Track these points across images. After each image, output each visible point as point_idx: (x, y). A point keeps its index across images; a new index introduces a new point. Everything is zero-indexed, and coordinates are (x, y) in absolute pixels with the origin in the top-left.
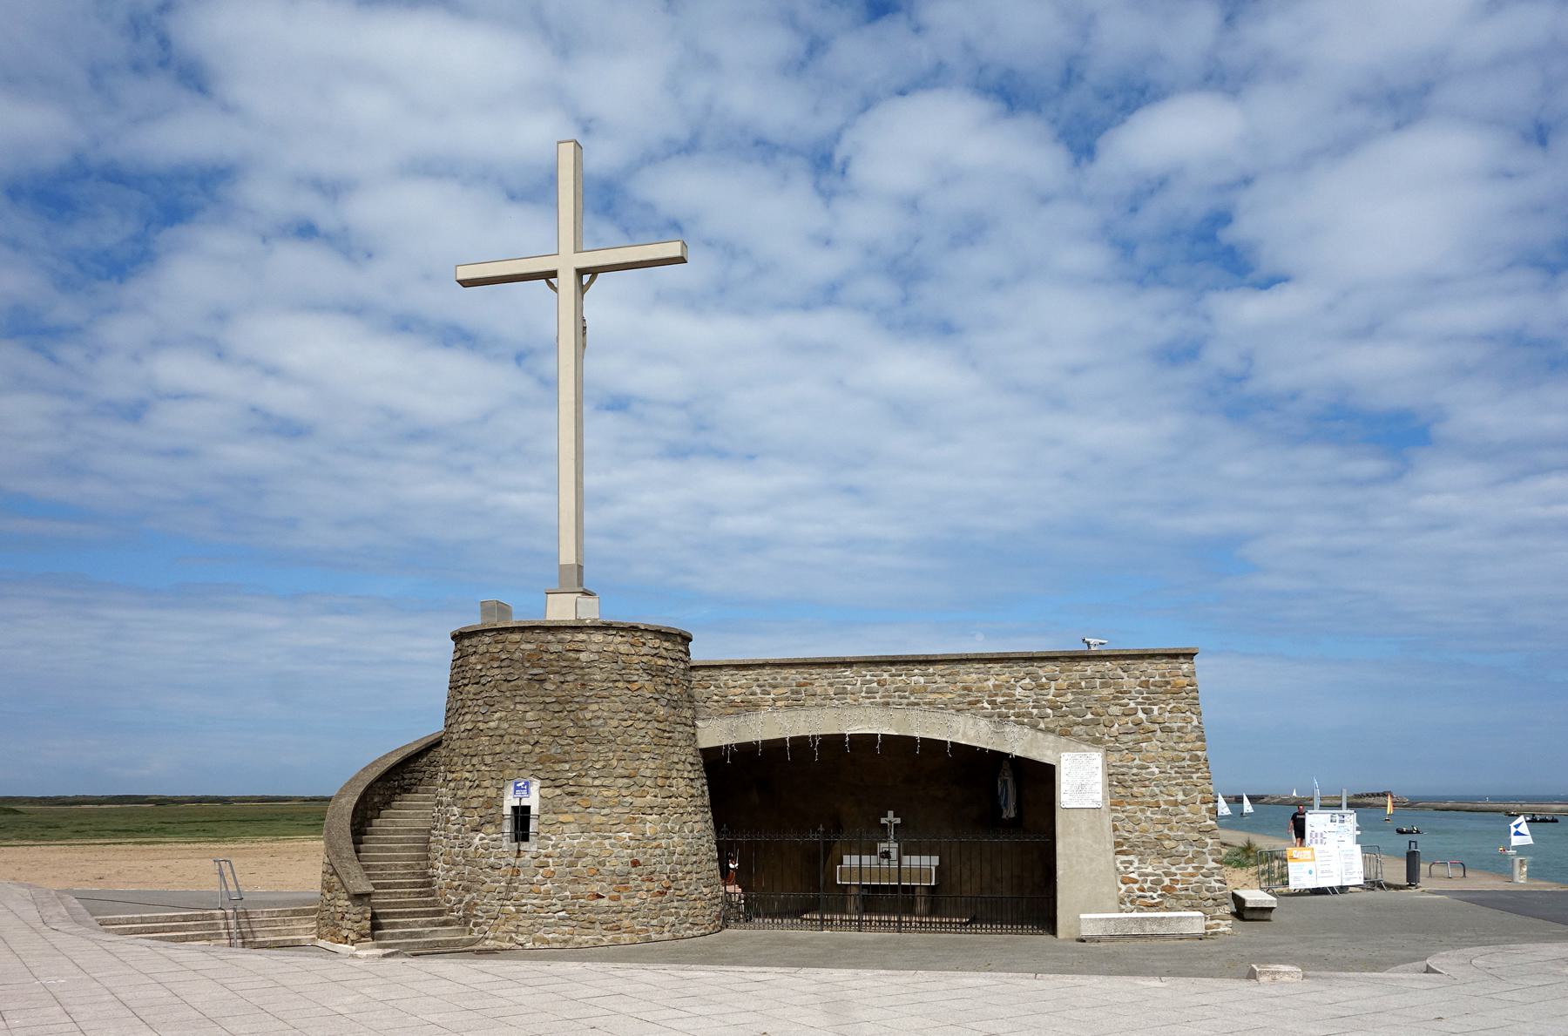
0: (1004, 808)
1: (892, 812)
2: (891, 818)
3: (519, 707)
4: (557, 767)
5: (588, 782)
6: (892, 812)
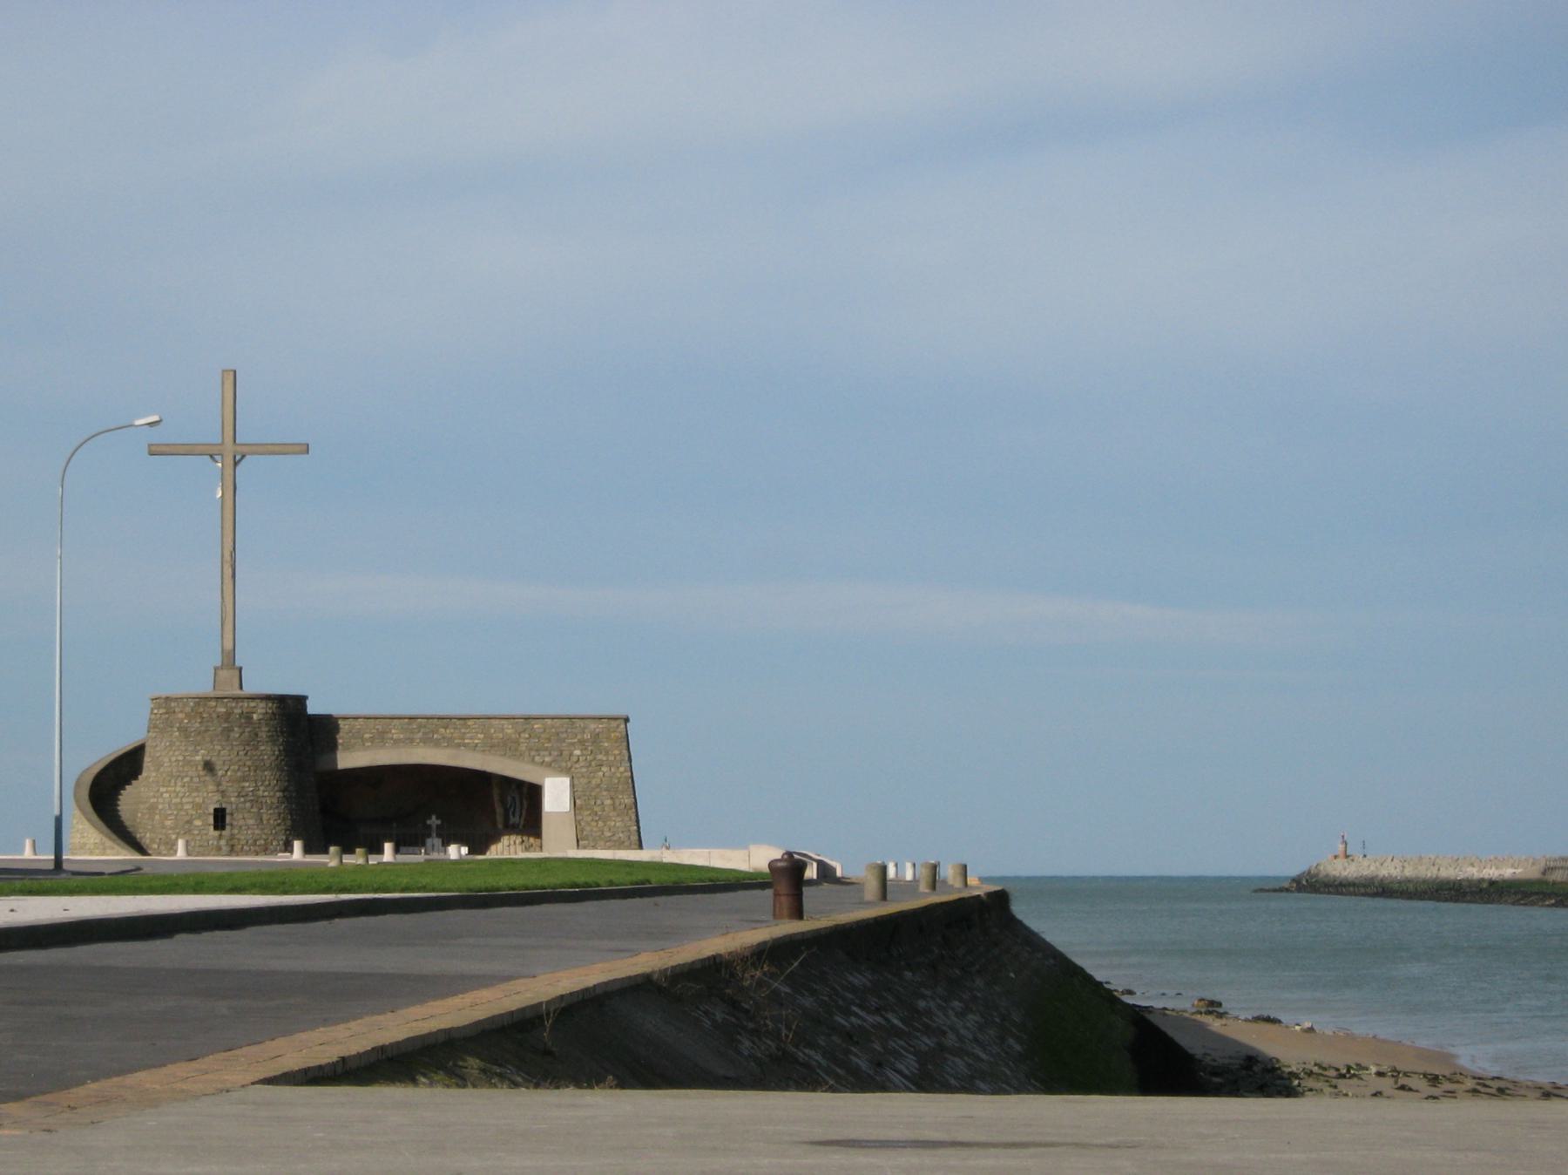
0: (511, 817)
1: (565, 782)
2: (434, 821)
6: (565, 782)
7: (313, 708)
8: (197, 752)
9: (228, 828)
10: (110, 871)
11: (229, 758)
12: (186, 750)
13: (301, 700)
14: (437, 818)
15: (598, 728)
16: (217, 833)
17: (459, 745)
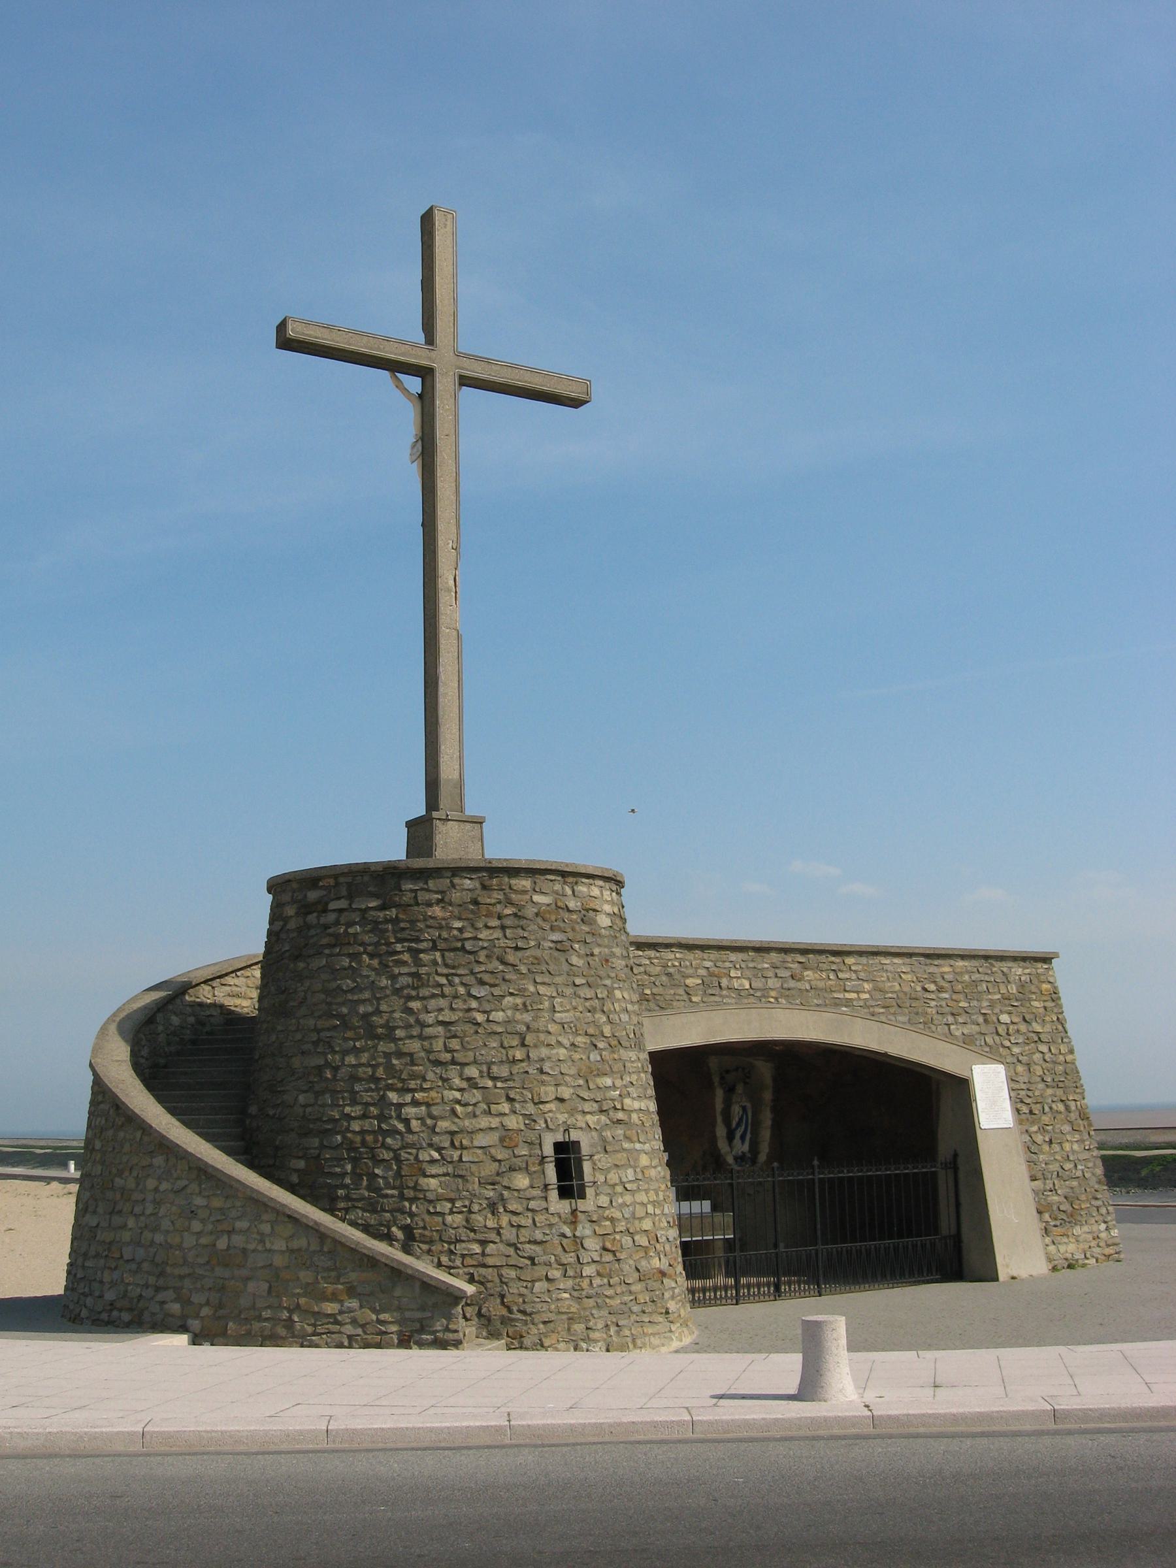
3: (542, 990)
17: (837, 1003)
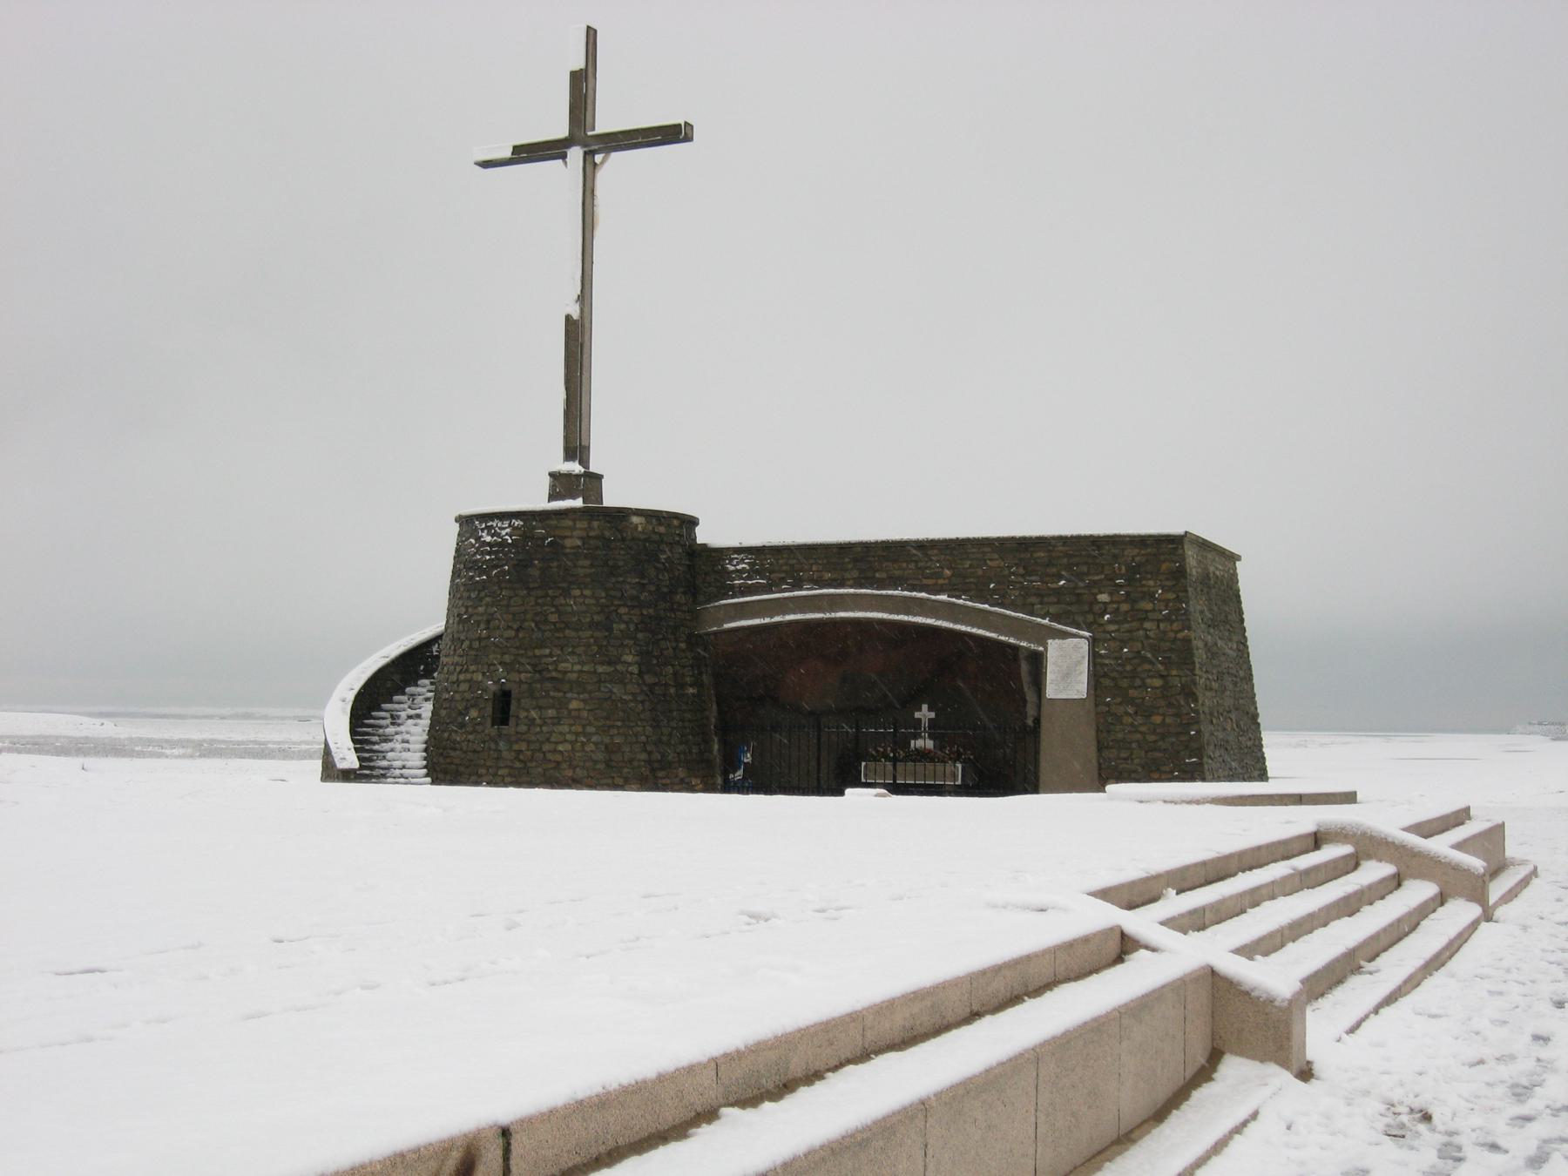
4: (537, 652)
5: (568, 668)
7: (703, 536)
8: (481, 600)
9: (512, 721)
10: (260, 771)
11: (523, 608)
12: (469, 597)
13: (691, 522)
14: (930, 709)
15: (1138, 555)
16: (493, 731)
